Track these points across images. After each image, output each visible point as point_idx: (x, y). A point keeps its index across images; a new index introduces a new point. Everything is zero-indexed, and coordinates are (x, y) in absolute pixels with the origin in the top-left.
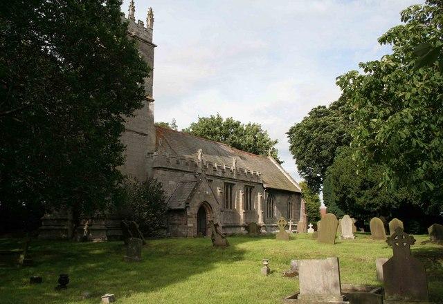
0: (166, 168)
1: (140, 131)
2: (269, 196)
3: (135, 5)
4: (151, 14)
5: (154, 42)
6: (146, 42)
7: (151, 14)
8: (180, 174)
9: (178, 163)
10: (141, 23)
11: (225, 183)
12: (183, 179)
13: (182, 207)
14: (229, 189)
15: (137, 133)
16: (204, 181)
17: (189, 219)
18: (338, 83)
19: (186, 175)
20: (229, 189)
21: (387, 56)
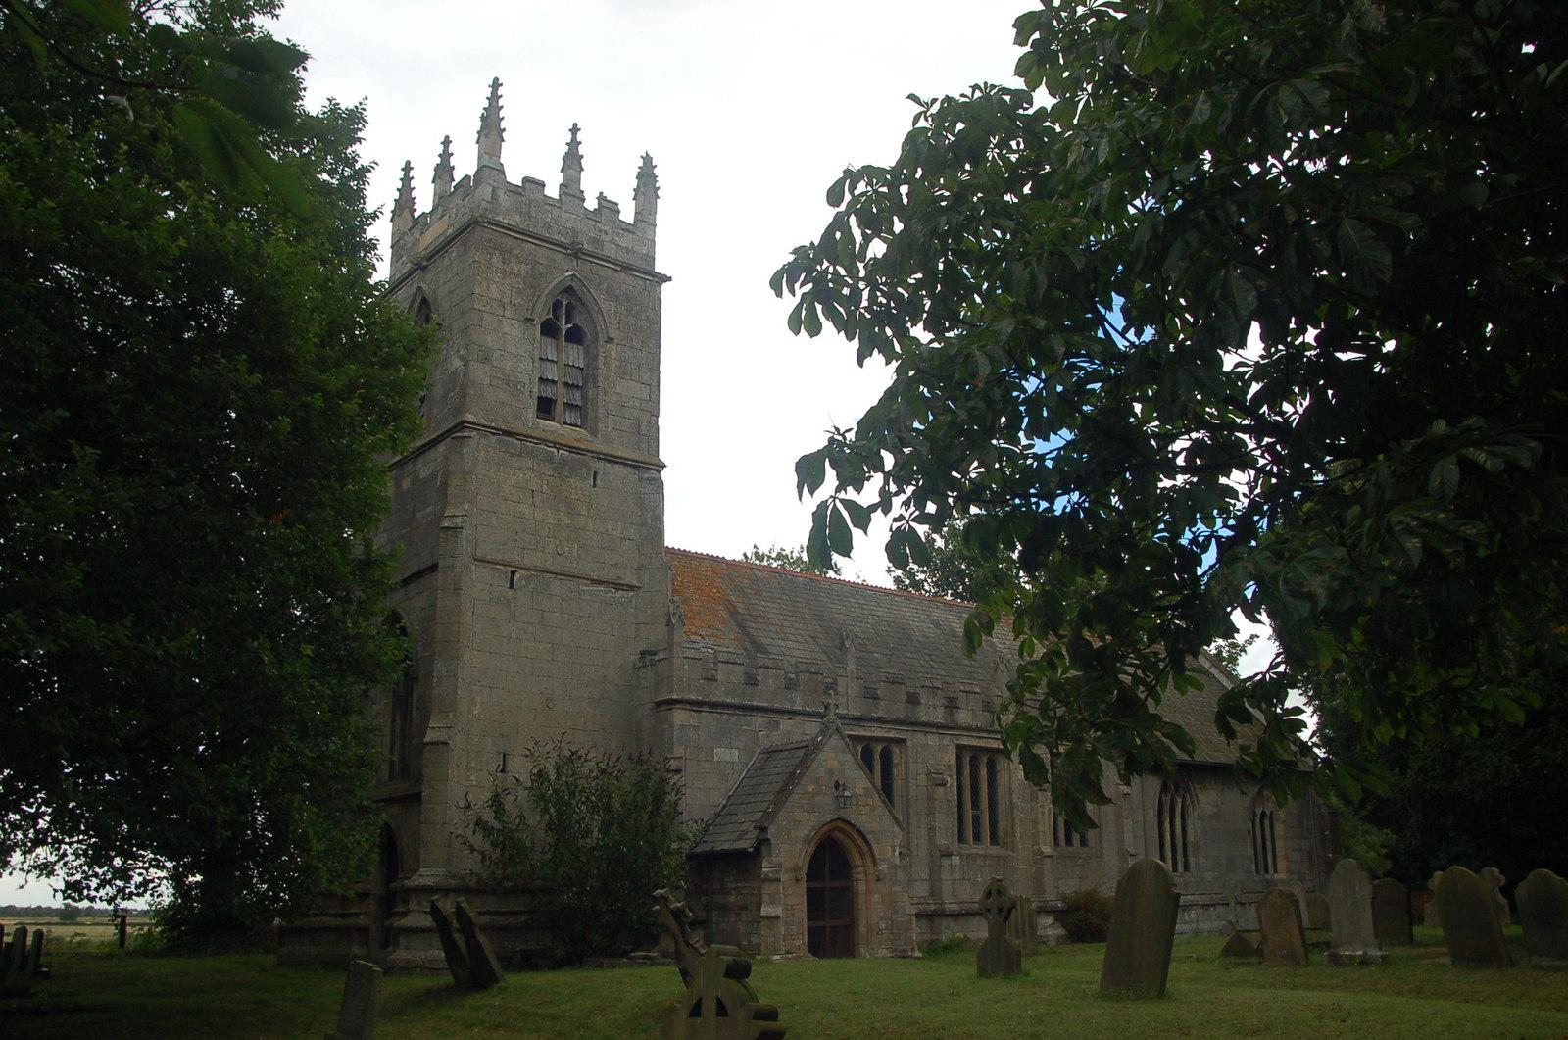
0: (700, 703)
1: (611, 574)
2: (1165, 788)
3: (580, 137)
4: (647, 181)
5: (660, 267)
6: (626, 268)
7: (647, 181)
8: (759, 721)
9: (751, 681)
10: (607, 206)
11: (960, 749)
12: (776, 739)
13: (747, 844)
14: (984, 772)
15: (599, 583)
16: (835, 741)
17: (768, 888)
18: (803, 322)
19: (786, 724)
20: (984, 772)
21: (360, 130)
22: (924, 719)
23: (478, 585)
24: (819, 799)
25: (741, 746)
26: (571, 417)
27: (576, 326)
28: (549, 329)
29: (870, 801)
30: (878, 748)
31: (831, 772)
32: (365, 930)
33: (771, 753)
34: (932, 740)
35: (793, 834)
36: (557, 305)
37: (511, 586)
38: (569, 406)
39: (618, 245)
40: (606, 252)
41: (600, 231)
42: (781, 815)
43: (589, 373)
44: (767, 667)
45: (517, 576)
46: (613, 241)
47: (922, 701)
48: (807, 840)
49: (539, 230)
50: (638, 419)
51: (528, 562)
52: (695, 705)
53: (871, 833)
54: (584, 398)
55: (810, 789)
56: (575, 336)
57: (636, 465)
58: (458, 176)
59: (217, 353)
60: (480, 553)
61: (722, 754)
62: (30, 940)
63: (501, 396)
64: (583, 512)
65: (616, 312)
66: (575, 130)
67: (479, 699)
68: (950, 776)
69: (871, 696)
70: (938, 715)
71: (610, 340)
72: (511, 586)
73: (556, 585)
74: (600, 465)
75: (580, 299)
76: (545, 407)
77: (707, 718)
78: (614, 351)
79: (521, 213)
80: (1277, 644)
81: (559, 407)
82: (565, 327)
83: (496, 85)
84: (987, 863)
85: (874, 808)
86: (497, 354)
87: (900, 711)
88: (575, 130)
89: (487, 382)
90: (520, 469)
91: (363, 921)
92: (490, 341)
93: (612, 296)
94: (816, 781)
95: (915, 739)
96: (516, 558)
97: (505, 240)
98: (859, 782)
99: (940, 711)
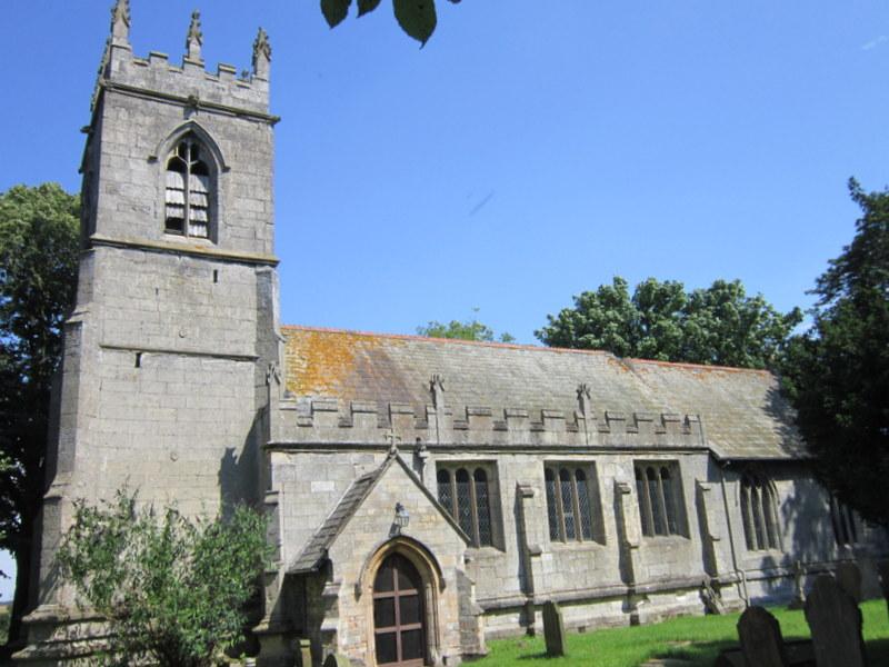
2: (744, 484)
8: (354, 456)
22: (511, 443)
24: (380, 520)
25: (337, 477)
26: (202, 231)
27: (201, 162)
28: (175, 165)
29: (433, 518)
30: (471, 471)
31: (393, 495)
34: (521, 459)
35: (355, 553)
37: (138, 365)
39: (234, 98)
40: (224, 103)
41: (218, 88)
43: (212, 196)
44: (361, 412)
45: (143, 356)
46: (230, 95)
47: (509, 428)
48: (369, 558)
49: (163, 91)
50: (254, 228)
51: (152, 345)
53: (435, 545)
55: (371, 512)
59: (733, 342)
60: (107, 342)
61: (319, 486)
63: (128, 218)
64: (205, 302)
65: (233, 148)
67: (106, 458)
68: (539, 487)
69: (461, 427)
70: (526, 438)
71: (226, 169)
72: (138, 365)
74: (219, 266)
75: (200, 140)
77: (304, 458)
78: (230, 176)
79: (146, 79)
82: (189, 164)
83: (806, 293)
84: (579, 556)
85: (437, 523)
86: (123, 186)
87: (489, 438)
89: (114, 208)
90: (145, 272)
92: (118, 176)
93: (231, 137)
94: (377, 504)
95: (504, 460)
96: (140, 343)
97: (130, 99)
99: (592, 416)
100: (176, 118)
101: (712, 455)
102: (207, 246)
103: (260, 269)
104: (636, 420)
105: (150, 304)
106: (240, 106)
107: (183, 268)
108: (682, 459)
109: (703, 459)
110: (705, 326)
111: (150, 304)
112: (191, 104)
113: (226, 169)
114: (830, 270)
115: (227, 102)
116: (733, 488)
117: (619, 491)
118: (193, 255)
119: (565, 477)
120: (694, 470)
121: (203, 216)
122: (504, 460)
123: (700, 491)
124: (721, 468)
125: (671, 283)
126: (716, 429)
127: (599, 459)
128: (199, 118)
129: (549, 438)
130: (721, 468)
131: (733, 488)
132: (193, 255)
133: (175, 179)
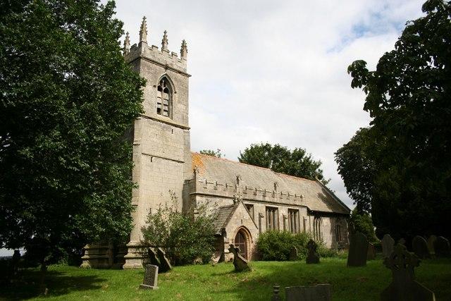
2: (315, 218)
12: (222, 205)
19: (224, 200)
23: (145, 160)
26: (165, 113)
28: (160, 89)
32: (107, 259)
33: (222, 208)
36: (161, 82)
38: (165, 110)
42: (229, 225)
43: (170, 101)
52: (201, 195)
54: (169, 108)
56: (166, 91)
57: (183, 128)
58: (132, 44)
62: (97, 284)
66: (165, 32)
71: (176, 93)
73: (163, 161)
74: (173, 128)
76: (159, 110)
80: (131, 35)
81: (162, 111)
87: (252, 197)
88: (144, 18)
91: (107, 256)
95: (256, 205)
98: (247, 216)
99: (262, 197)
100: (163, 72)
101: (308, 209)
102: (168, 119)
103: (186, 131)
104: (289, 195)
105: (155, 139)
106: (178, 69)
107: (164, 127)
108: (300, 209)
109: (306, 209)
110: (17, 21)
111: (155, 139)
112: (167, 67)
113: (176, 93)
114: (366, 90)
115: (175, 67)
116: (312, 218)
117: (284, 218)
118: (167, 123)
119: (270, 211)
120: (303, 213)
121: (166, 108)
122: (256, 205)
123: (304, 220)
124: (310, 212)
125: (306, 155)
126: (272, 253)
127: (279, 207)
128: (168, 72)
129: (267, 199)
130: (310, 212)
131: (312, 218)
132: (167, 123)
133: (159, 94)
